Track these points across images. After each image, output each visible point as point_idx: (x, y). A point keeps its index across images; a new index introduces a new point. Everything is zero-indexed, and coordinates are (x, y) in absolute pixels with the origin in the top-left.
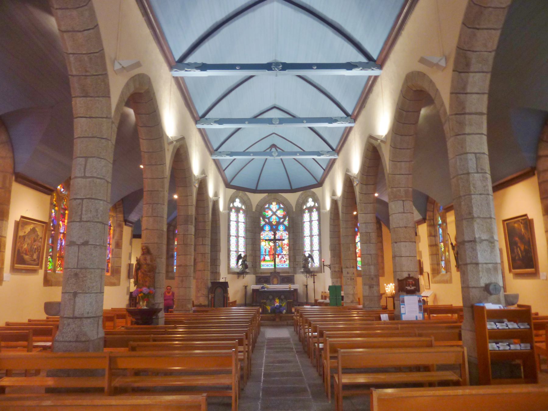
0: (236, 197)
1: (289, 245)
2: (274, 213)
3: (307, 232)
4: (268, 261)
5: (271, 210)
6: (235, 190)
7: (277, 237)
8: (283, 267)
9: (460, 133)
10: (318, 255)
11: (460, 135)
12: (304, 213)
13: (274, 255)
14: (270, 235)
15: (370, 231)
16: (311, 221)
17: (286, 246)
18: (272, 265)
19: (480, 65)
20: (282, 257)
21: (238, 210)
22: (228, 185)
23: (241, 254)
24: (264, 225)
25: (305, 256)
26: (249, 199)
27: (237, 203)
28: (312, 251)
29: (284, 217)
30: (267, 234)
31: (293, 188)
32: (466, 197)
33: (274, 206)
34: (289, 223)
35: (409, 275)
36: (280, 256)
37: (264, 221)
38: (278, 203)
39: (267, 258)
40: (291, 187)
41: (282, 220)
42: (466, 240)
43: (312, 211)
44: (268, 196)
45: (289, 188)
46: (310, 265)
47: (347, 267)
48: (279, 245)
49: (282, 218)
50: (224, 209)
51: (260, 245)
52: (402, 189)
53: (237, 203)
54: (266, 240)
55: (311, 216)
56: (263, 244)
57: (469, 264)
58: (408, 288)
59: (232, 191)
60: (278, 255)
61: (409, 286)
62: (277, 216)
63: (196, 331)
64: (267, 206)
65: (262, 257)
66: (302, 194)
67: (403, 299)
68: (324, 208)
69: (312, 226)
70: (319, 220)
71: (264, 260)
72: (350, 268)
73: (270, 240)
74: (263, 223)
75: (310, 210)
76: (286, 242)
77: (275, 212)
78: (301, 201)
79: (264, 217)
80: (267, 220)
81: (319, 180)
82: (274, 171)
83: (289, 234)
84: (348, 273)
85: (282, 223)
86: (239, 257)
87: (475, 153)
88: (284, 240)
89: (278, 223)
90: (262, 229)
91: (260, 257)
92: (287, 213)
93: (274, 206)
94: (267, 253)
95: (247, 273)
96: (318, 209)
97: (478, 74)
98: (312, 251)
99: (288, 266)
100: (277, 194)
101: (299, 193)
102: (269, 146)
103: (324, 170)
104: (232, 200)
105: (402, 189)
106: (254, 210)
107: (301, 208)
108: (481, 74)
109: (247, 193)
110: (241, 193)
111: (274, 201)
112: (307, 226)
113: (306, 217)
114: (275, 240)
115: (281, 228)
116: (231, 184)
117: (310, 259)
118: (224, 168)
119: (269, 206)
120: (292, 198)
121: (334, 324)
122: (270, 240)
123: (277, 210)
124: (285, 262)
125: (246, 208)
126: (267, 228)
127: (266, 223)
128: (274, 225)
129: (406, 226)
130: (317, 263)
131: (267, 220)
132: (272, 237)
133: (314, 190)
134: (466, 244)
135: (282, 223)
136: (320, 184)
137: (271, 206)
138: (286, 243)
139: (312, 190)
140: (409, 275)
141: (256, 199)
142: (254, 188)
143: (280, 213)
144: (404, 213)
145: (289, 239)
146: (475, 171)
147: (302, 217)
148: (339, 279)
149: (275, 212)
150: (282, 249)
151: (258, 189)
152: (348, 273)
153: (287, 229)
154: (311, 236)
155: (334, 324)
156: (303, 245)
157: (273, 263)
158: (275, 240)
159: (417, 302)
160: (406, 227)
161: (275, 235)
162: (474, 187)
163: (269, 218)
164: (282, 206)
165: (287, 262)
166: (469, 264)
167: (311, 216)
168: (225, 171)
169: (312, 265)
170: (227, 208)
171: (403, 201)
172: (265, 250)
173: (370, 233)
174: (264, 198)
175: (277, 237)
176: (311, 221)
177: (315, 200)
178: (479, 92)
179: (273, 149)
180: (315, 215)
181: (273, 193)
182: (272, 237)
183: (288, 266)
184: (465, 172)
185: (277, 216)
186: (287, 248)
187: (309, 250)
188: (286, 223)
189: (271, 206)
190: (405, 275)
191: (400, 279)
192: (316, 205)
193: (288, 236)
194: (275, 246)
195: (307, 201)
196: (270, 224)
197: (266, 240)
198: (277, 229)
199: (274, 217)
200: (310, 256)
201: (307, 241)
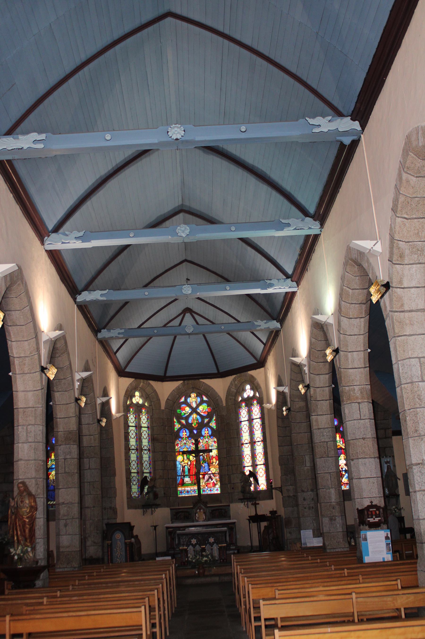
0: (136, 389)
1: (219, 457)
2: (194, 410)
3: (245, 437)
4: (188, 485)
5: (190, 406)
6: (132, 380)
7: (201, 446)
8: (212, 492)
9: (400, 334)
10: (263, 472)
11: (402, 336)
12: (240, 407)
13: (197, 474)
14: (190, 445)
15: (327, 440)
16: (250, 420)
17: (214, 460)
18: (194, 491)
19: (416, 256)
20: (210, 478)
21: (138, 408)
22: (121, 372)
23: (146, 477)
24: (179, 430)
25: (244, 473)
26: (155, 391)
27: (137, 399)
28: (254, 465)
29: (210, 416)
30: (185, 443)
31: (221, 370)
32: (411, 410)
33: (193, 400)
34: (217, 424)
35: (371, 502)
36: (207, 477)
37: (179, 422)
38: (199, 395)
39: (187, 480)
40: (218, 369)
41: (206, 420)
42: (413, 463)
43: (252, 404)
44: (183, 385)
45: (216, 371)
46: (252, 488)
47: (303, 491)
48: (204, 460)
49: (206, 417)
50: (118, 411)
51: (175, 461)
52: (357, 388)
53: (137, 399)
54: (184, 453)
55: (250, 412)
56: (180, 458)
57: (419, 491)
58: (371, 520)
59: (127, 382)
60: (204, 475)
61: (372, 517)
62: (198, 414)
63: (327, 618)
64: (183, 400)
65: (179, 481)
66: (234, 380)
67: (366, 535)
68: (269, 402)
69: (251, 427)
70: (262, 418)
71: (183, 484)
72: (308, 491)
73: (189, 453)
74: (177, 426)
75: (249, 402)
76: (214, 453)
77: (195, 407)
78: (234, 390)
79: (179, 417)
80: (183, 421)
81: (258, 357)
82: (189, 351)
83: (218, 442)
84: (304, 499)
85: (207, 425)
86: (143, 482)
87: (419, 358)
88: (211, 451)
89: (201, 425)
90: (177, 436)
91: (176, 480)
92: (214, 409)
93: (193, 400)
94: (187, 473)
95: (158, 506)
96: (260, 402)
97: (415, 266)
98: (254, 465)
99: (219, 492)
100: (197, 381)
101: (230, 379)
102: (180, 312)
103: (265, 344)
104: (130, 395)
105: (357, 388)
106: (163, 407)
107: (236, 400)
108: (418, 265)
109: (152, 382)
110: (142, 383)
111: (193, 392)
112: (245, 427)
113: (244, 414)
114: (197, 452)
115: (205, 432)
116: (127, 370)
117: (252, 479)
118: (115, 351)
119: (186, 400)
120: (220, 386)
121: (164, 603)
122: (189, 453)
123: (198, 406)
124: (214, 485)
125: (150, 405)
126: (184, 434)
127: (183, 427)
128: (194, 429)
129: (364, 436)
130: (263, 485)
131: (183, 421)
132: (193, 447)
133: (251, 372)
134: (414, 467)
135: (207, 425)
136: (261, 363)
137: (189, 400)
138: (214, 456)
139: (250, 373)
140: (371, 502)
141: (165, 390)
142: (162, 374)
143: (203, 408)
144: (361, 419)
145: (218, 448)
146: (420, 379)
147: (237, 414)
148: (296, 508)
149: (195, 407)
150: (210, 464)
151: (168, 374)
152: (304, 499)
153: (214, 434)
154: (252, 443)
155: (164, 603)
156: (241, 457)
157: (196, 488)
158: (197, 452)
159: (384, 539)
160: (364, 439)
161: (197, 443)
162: (419, 399)
163: (187, 418)
164: (205, 399)
165: (218, 486)
166: (419, 491)
167: (250, 412)
168: (118, 354)
169: (255, 488)
170: (122, 409)
171: (359, 403)
172: (184, 467)
173: (327, 442)
174: (178, 388)
175: (201, 446)
176: (250, 420)
177: (255, 388)
178: (418, 286)
179: (188, 315)
180: (256, 411)
181: (191, 380)
182: (193, 447)
183: (219, 492)
184: (409, 381)
185: (198, 414)
186: (215, 462)
187: (250, 464)
188: (213, 424)
189: (189, 400)
190: (367, 503)
191: (360, 508)
192: (257, 395)
193: (216, 445)
194: (198, 461)
195: (244, 390)
196: (188, 426)
197: (184, 453)
198: (200, 435)
199: (194, 416)
200: (253, 474)
201: (247, 451)
